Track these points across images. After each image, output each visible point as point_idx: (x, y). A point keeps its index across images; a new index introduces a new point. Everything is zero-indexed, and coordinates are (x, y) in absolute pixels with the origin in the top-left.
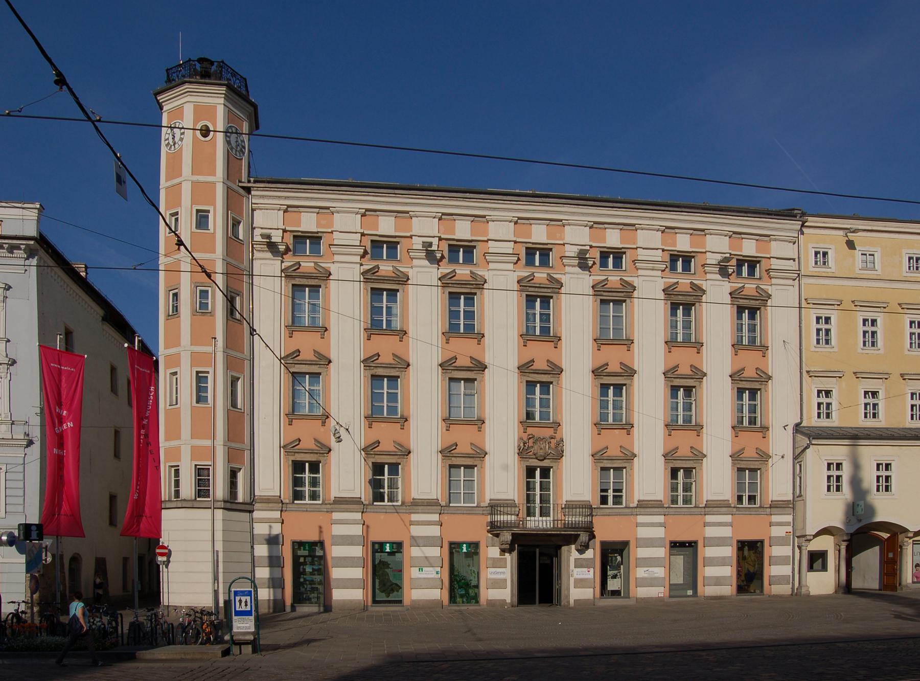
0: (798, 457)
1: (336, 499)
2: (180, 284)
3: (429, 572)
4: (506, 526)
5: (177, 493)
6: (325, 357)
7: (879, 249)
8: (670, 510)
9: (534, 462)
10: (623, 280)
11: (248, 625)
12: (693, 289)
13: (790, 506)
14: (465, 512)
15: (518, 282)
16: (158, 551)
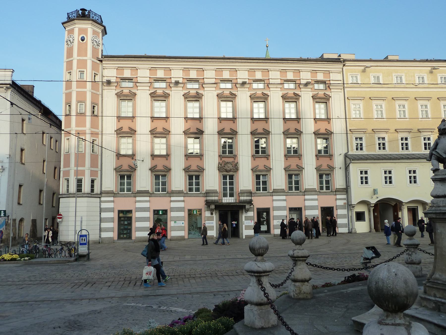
0: (347, 168)
1: (207, 191)
2: (71, 102)
3: (179, 223)
4: (213, 202)
5: (92, 191)
6: (133, 130)
7: (404, 74)
8: (288, 193)
9: (225, 173)
10: (295, 93)
11: (85, 249)
12: (295, 95)
13: (345, 191)
14: (195, 196)
15: (217, 95)
16: (58, 216)
